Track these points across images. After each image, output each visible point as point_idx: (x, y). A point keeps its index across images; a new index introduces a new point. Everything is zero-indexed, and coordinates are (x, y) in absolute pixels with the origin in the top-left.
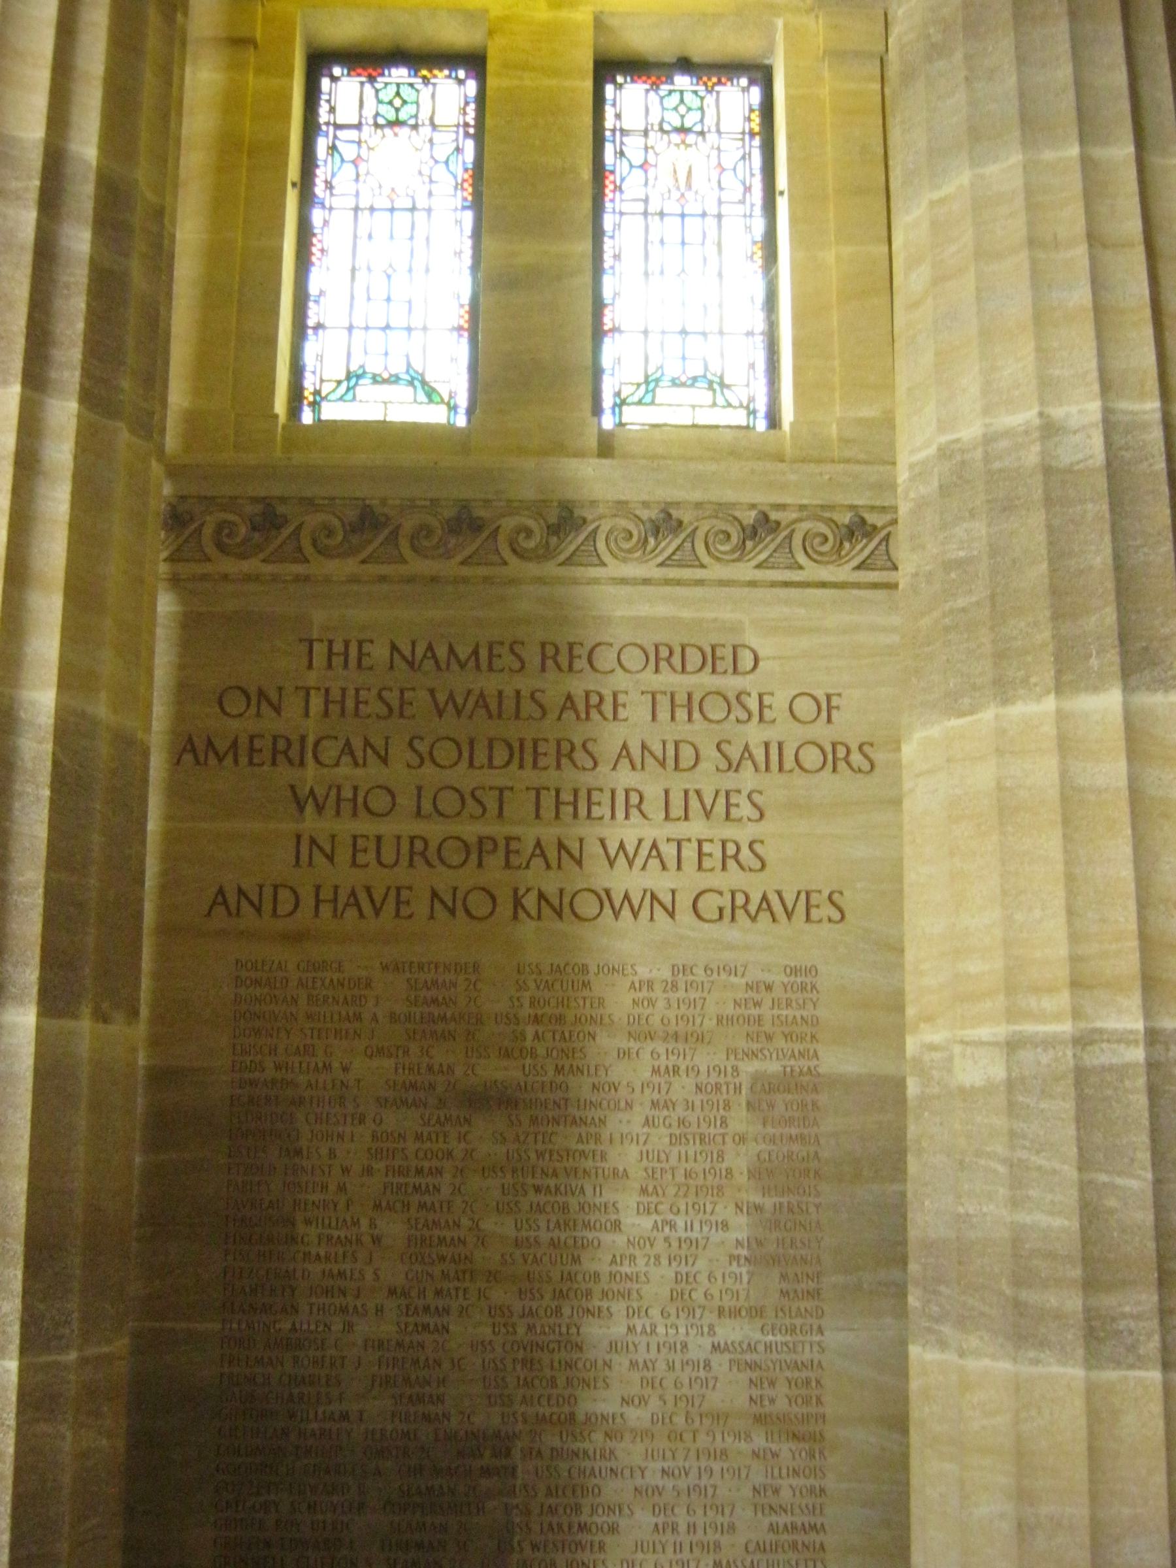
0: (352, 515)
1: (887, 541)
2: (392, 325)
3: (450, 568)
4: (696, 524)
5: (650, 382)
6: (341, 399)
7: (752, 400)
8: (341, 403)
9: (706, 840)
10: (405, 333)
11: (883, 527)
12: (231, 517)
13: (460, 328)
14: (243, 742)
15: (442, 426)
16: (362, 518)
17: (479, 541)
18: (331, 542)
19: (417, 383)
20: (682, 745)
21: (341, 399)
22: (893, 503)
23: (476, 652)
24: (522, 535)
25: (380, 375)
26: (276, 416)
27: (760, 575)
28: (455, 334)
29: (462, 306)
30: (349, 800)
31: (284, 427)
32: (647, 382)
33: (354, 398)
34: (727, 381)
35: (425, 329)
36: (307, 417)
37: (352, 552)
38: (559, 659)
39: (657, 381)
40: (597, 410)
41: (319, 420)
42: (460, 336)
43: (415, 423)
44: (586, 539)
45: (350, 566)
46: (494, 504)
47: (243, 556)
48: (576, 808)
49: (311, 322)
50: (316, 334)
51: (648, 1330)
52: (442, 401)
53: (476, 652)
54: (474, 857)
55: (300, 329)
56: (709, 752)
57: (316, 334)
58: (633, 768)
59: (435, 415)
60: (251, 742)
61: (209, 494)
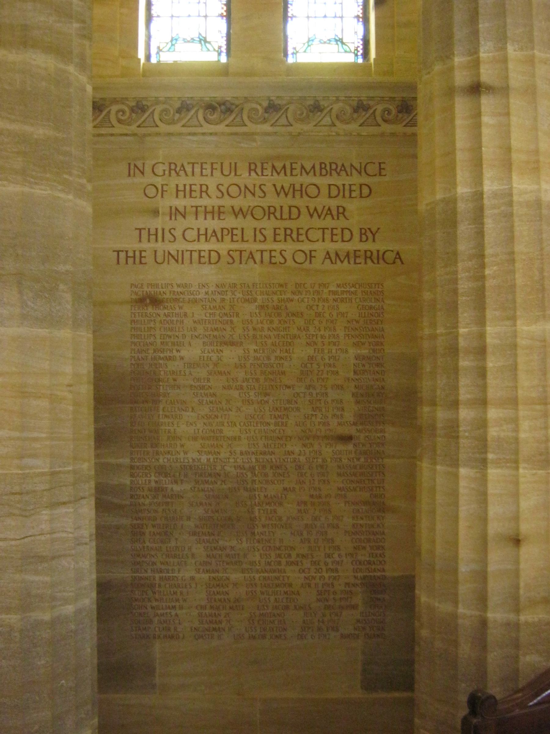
0: (265, 104)
1: (287, 112)
2: (327, 16)
3: (176, 128)
4: (331, 107)
5: (173, 41)
6: (168, 51)
7: (220, 47)
8: (168, 53)
9: (143, 251)
10: (204, 18)
11: (328, 106)
12: (168, 107)
13: (358, 17)
14: (216, 209)
15: (352, 63)
16: (137, 106)
17: (323, 115)
18: (391, 117)
19: (203, 42)
20: (292, 208)
21: (168, 51)
22: (416, 96)
23: (313, 167)
24: (121, 113)
25: (186, 39)
26: (139, 60)
27: (185, 130)
28: (356, 20)
29: (359, 6)
30: (152, 235)
31: (144, 64)
32: (172, 41)
33: (174, 51)
34: (208, 40)
35: (308, 17)
36: (154, 60)
37: (265, 121)
38: (257, 170)
39: (176, 40)
40: (286, 55)
41: (160, 61)
42: (358, 21)
43: (208, 61)
44: (149, 116)
45: (266, 127)
46: (173, 99)
47: (129, 124)
48: (157, 237)
49: (289, 15)
50: (292, 19)
51: (175, 461)
52: (214, 50)
53: (313, 167)
54: (381, 256)
55: (149, 18)
56: (304, 210)
57: (292, 19)
58: (333, 219)
59: (212, 57)
60: (219, 209)
61: (169, 96)
